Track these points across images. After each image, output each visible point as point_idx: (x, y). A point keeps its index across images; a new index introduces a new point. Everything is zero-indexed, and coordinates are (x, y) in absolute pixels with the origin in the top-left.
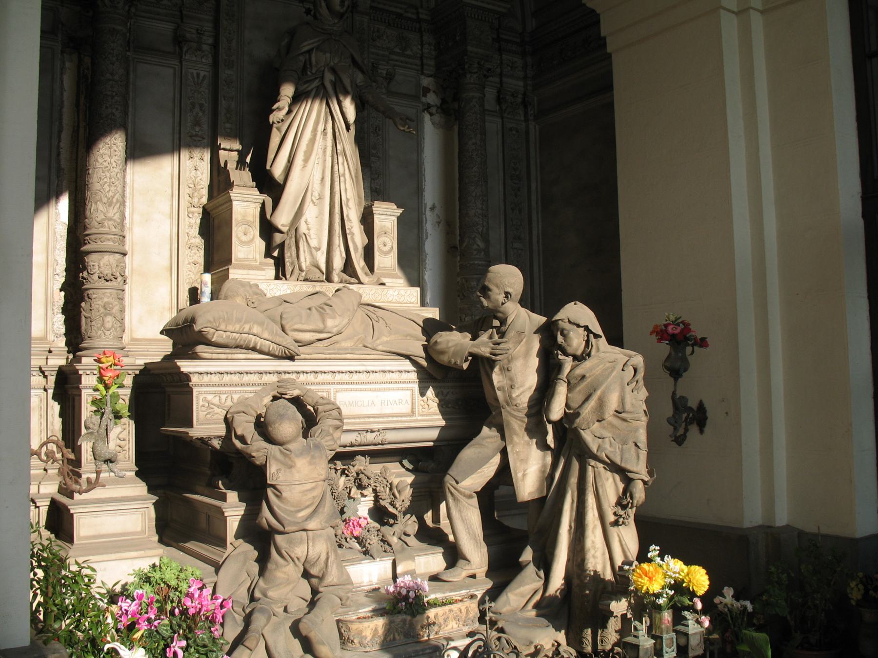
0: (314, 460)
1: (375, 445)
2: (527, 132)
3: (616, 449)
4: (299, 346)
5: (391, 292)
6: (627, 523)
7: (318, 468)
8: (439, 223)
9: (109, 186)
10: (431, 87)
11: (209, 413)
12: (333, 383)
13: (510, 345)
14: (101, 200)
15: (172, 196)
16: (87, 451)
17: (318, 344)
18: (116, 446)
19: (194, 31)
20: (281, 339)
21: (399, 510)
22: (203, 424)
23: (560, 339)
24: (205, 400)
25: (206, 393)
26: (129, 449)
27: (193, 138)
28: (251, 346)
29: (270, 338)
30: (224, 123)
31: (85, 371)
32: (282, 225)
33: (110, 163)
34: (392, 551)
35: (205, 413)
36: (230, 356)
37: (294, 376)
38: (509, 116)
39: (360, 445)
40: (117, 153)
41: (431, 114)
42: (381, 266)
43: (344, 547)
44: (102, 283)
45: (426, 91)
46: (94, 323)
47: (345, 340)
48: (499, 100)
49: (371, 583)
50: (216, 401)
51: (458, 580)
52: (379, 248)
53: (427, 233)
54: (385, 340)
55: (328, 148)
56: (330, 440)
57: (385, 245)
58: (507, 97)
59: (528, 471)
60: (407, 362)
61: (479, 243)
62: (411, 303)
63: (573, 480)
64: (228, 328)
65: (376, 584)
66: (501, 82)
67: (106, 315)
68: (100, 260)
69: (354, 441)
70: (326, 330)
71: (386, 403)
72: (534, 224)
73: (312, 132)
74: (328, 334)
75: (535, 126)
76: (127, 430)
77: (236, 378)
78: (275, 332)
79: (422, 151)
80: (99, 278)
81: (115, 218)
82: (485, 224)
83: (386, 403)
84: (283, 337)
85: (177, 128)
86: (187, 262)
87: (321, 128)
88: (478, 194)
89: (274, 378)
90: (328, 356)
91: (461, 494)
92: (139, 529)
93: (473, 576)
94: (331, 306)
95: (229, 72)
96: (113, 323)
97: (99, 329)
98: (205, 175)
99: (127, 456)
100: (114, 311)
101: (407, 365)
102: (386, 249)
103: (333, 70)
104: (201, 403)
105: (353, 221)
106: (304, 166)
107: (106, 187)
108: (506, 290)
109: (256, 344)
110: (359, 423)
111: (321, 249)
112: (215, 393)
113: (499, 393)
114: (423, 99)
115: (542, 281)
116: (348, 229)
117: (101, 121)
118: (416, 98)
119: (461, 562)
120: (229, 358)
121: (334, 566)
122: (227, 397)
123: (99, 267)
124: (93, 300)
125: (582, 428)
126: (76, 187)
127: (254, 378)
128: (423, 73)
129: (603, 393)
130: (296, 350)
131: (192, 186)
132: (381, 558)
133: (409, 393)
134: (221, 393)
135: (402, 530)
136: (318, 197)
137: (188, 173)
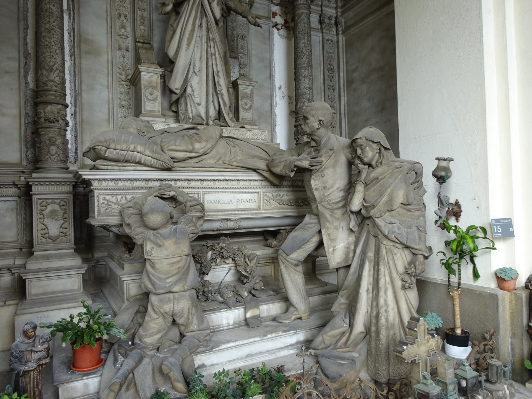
0: (179, 241)
1: (234, 229)
2: (338, 42)
3: (402, 231)
4: (174, 162)
5: (249, 132)
6: (412, 288)
7: (182, 246)
8: (284, 97)
9: (50, 58)
10: (277, 12)
11: (108, 209)
13: (323, 159)
14: (44, 67)
15: (108, 74)
16: (38, 236)
18: (60, 233)
20: (159, 156)
21: (249, 273)
22: (102, 216)
23: (359, 151)
24: (104, 199)
25: (104, 194)
26: (70, 234)
27: (121, 36)
28: (137, 161)
29: (151, 155)
30: (139, 26)
31: (34, 183)
32: (176, 89)
33: (50, 42)
34: (243, 302)
35: (105, 208)
37: (172, 183)
38: (327, 32)
39: (223, 230)
40: (55, 36)
41: (278, 29)
42: (244, 118)
43: (210, 300)
44: (47, 124)
45: (275, 14)
46: (43, 151)
47: (210, 158)
48: (321, 22)
49: (228, 325)
50: (113, 200)
51: (289, 322)
52: (242, 106)
53: (276, 103)
54: (240, 157)
55: (204, 36)
56: (193, 226)
57: (246, 105)
58: (326, 20)
59: (336, 247)
60: (255, 174)
62: (262, 140)
63: (371, 254)
64: (117, 147)
65: (232, 325)
66: (322, 11)
67: (51, 145)
68: (45, 108)
69: (219, 227)
70: (195, 151)
71: (240, 202)
72: (342, 98)
73: (192, 25)
74: (196, 154)
75: (343, 38)
76: (68, 222)
77: (128, 184)
78: (154, 150)
79: (273, 52)
80: (45, 120)
81: (55, 80)
82: (311, 93)
84: (161, 154)
85: (109, 30)
86: (119, 116)
87: (198, 22)
88: (306, 75)
89: (157, 184)
90: (197, 169)
91: (290, 263)
92: (76, 288)
93: (300, 318)
94: (199, 135)
96: (56, 151)
97: (46, 155)
98: (130, 61)
99: (68, 239)
100: (57, 143)
101: (254, 176)
102: (247, 107)
104: (102, 201)
105: (222, 86)
106: (188, 48)
107: (47, 59)
108: (319, 119)
109: (140, 159)
110: (223, 215)
111: (202, 104)
112: (112, 194)
113: (316, 193)
114: (273, 20)
115: (347, 132)
116: (219, 90)
117: (42, 13)
118: (268, 18)
119: (291, 309)
120: (121, 169)
121: (195, 318)
122: (122, 197)
123: (45, 113)
124: (42, 136)
125: (376, 216)
127: (143, 184)
129: (392, 191)
130: (172, 165)
131: (121, 68)
132: (235, 307)
133: (256, 195)
134: (117, 194)
135: (251, 287)
136: (198, 70)
137: (118, 60)
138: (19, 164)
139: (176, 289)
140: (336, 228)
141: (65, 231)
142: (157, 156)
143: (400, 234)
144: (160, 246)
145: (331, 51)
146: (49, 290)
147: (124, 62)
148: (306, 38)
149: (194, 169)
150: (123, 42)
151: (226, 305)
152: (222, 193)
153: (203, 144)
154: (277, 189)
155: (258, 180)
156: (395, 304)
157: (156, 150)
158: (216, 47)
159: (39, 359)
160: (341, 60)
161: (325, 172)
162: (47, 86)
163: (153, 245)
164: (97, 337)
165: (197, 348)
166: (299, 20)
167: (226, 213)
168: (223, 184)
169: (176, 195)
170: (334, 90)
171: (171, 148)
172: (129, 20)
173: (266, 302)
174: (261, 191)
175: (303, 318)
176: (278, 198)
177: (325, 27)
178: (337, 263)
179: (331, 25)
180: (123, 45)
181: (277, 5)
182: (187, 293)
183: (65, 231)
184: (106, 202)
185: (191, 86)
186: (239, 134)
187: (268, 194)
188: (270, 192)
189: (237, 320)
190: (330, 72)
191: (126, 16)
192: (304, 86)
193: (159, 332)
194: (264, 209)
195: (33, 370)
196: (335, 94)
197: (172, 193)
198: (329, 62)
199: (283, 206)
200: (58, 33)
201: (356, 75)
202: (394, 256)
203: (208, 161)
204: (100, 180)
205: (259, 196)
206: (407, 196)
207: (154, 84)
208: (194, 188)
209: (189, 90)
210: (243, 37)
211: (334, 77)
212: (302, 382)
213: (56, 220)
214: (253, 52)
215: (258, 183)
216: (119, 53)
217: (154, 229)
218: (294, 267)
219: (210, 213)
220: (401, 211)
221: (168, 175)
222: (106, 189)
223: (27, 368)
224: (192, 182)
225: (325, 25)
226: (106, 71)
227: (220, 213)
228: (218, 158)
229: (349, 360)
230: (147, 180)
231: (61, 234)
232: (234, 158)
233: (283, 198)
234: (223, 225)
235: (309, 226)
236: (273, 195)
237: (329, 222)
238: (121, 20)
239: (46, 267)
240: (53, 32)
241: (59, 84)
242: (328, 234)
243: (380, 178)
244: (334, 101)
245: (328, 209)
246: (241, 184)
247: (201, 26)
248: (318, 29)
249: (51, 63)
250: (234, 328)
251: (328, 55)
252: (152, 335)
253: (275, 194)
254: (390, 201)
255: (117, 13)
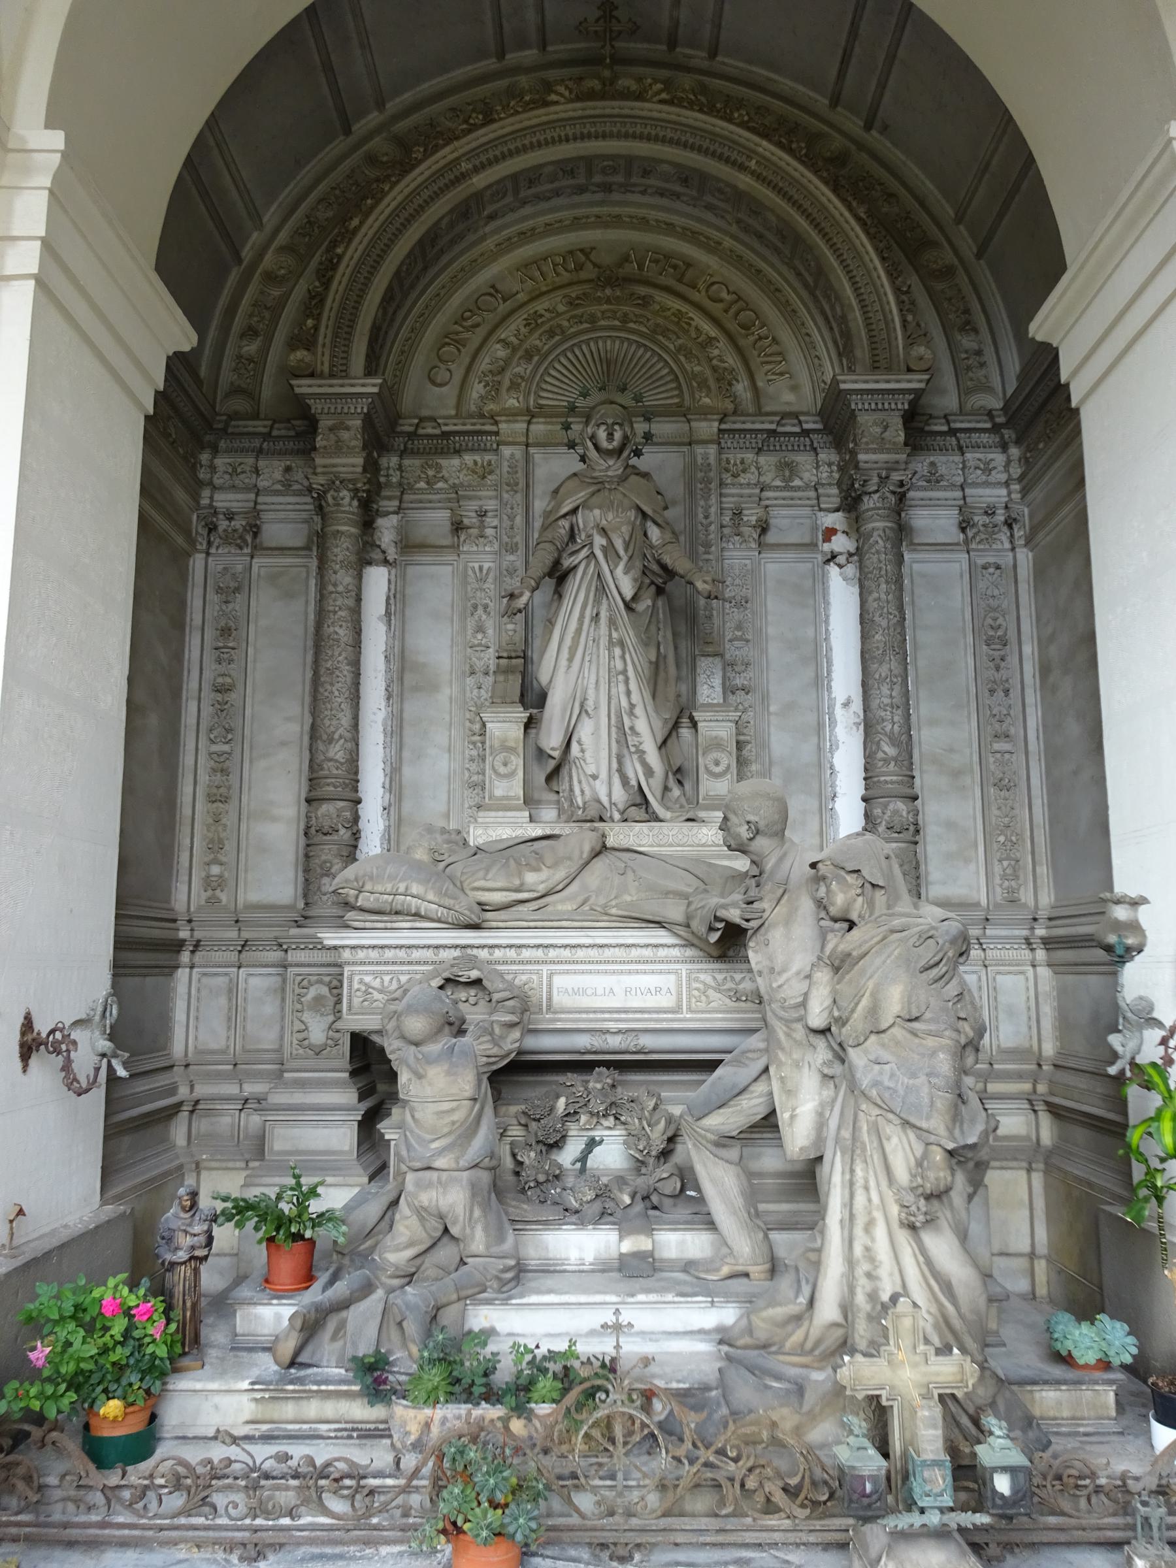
5: (705, 830)
7: (459, 1081)
10: (837, 527)
12: (545, 962)
17: (521, 908)
19: (474, 514)
20: (452, 902)
22: (356, 1014)
24: (361, 982)
25: (361, 973)
29: (436, 900)
32: (553, 749)
36: (389, 925)
39: (595, 1053)
41: (840, 566)
45: (830, 533)
50: (376, 983)
58: (976, 519)
59: (798, 1111)
60: (662, 932)
61: (886, 748)
71: (633, 992)
81: (337, 757)
83: (633, 992)
86: (466, 806)
88: (883, 675)
89: (457, 953)
90: (532, 924)
92: (346, 1148)
95: (512, 558)
101: (661, 936)
103: (604, 531)
104: (356, 986)
106: (569, 667)
107: (327, 722)
109: (418, 908)
110: (591, 1020)
112: (373, 973)
114: (826, 547)
118: (812, 546)
126: (314, 728)
127: (428, 954)
128: (821, 510)
138: (290, 907)
139: (440, 1163)
140: (797, 1065)
141: (337, 1035)
142: (448, 902)
143: (889, 1088)
144: (420, 1077)
145: (996, 592)
146: (302, 1146)
147: (479, 698)
148: (883, 586)
149: (525, 924)
150: (479, 659)
151: (573, 1215)
152: (591, 972)
153: (545, 874)
154: (723, 966)
155: (674, 946)
156: (894, 1262)
157: (447, 889)
158: (627, 657)
159: (193, 1248)
160: (1024, 613)
161: (770, 936)
162: (322, 769)
163: (411, 1075)
164: (293, 1230)
165: (477, 1290)
166: (866, 548)
167: (599, 1016)
168: (593, 953)
169: (482, 977)
170: (1007, 692)
171: (476, 884)
172: (492, 614)
173: (675, 1225)
174: (684, 969)
175: (752, 1275)
176: (730, 985)
177: (974, 537)
178: (801, 1149)
179: (996, 526)
180: (479, 665)
181: (837, 510)
182: (466, 1174)
183: (337, 1035)
184: (363, 988)
185: (579, 742)
186: (680, 837)
187: (702, 977)
188: (706, 971)
189: (604, 1255)
190: (993, 647)
191: (486, 607)
192: (878, 701)
193: (410, 1244)
194: (690, 1010)
195: (185, 1263)
196: (1011, 702)
197: (474, 974)
198: (989, 621)
199: (743, 1004)
200: (345, 673)
201: (1053, 650)
202: (885, 1142)
203: (560, 907)
204: (353, 947)
205: (679, 979)
206: (908, 1001)
207: (512, 744)
208: (529, 962)
209: (575, 748)
210: (742, 603)
211: (1008, 659)
212: (610, 1387)
213: (322, 1015)
214: (771, 631)
215: (676, 952)
216: (470, 681)
217: (417, 1044)
218: (713, 1149)
219: (563, 1016)
220: (896, 1032)
221: (475, 938)
222: (363, 963)
223: (174, 1258)
224: (524, 950)
225: (975, 530)
226: (447, 718)
227: (584, 1016)
228: (580, 899)
229: (789, 1382)
230: (437, 947)
231: (330, 1042)
232: (616, 898)
233: (741, 986)
234: (596, 1042)
235: (750, 1055)
236: (715, 978)
237: (783, 1049)
238: (476, 617)
239: (299, 1101)
240: (337, 673)
241: (342, 764)
242: (782, 1078)
243: (855, 953)
244: (1009, 720)
245: (780, 1019)
246: (635, 953)
247: (596, 617)
248: (957, 544)
249: (332, 729)
250: (593, 1271)
251: (988, 606)
252: (398, 1249)
253: (720, 977)
254: (874, 1011)
255: (469, 604)
